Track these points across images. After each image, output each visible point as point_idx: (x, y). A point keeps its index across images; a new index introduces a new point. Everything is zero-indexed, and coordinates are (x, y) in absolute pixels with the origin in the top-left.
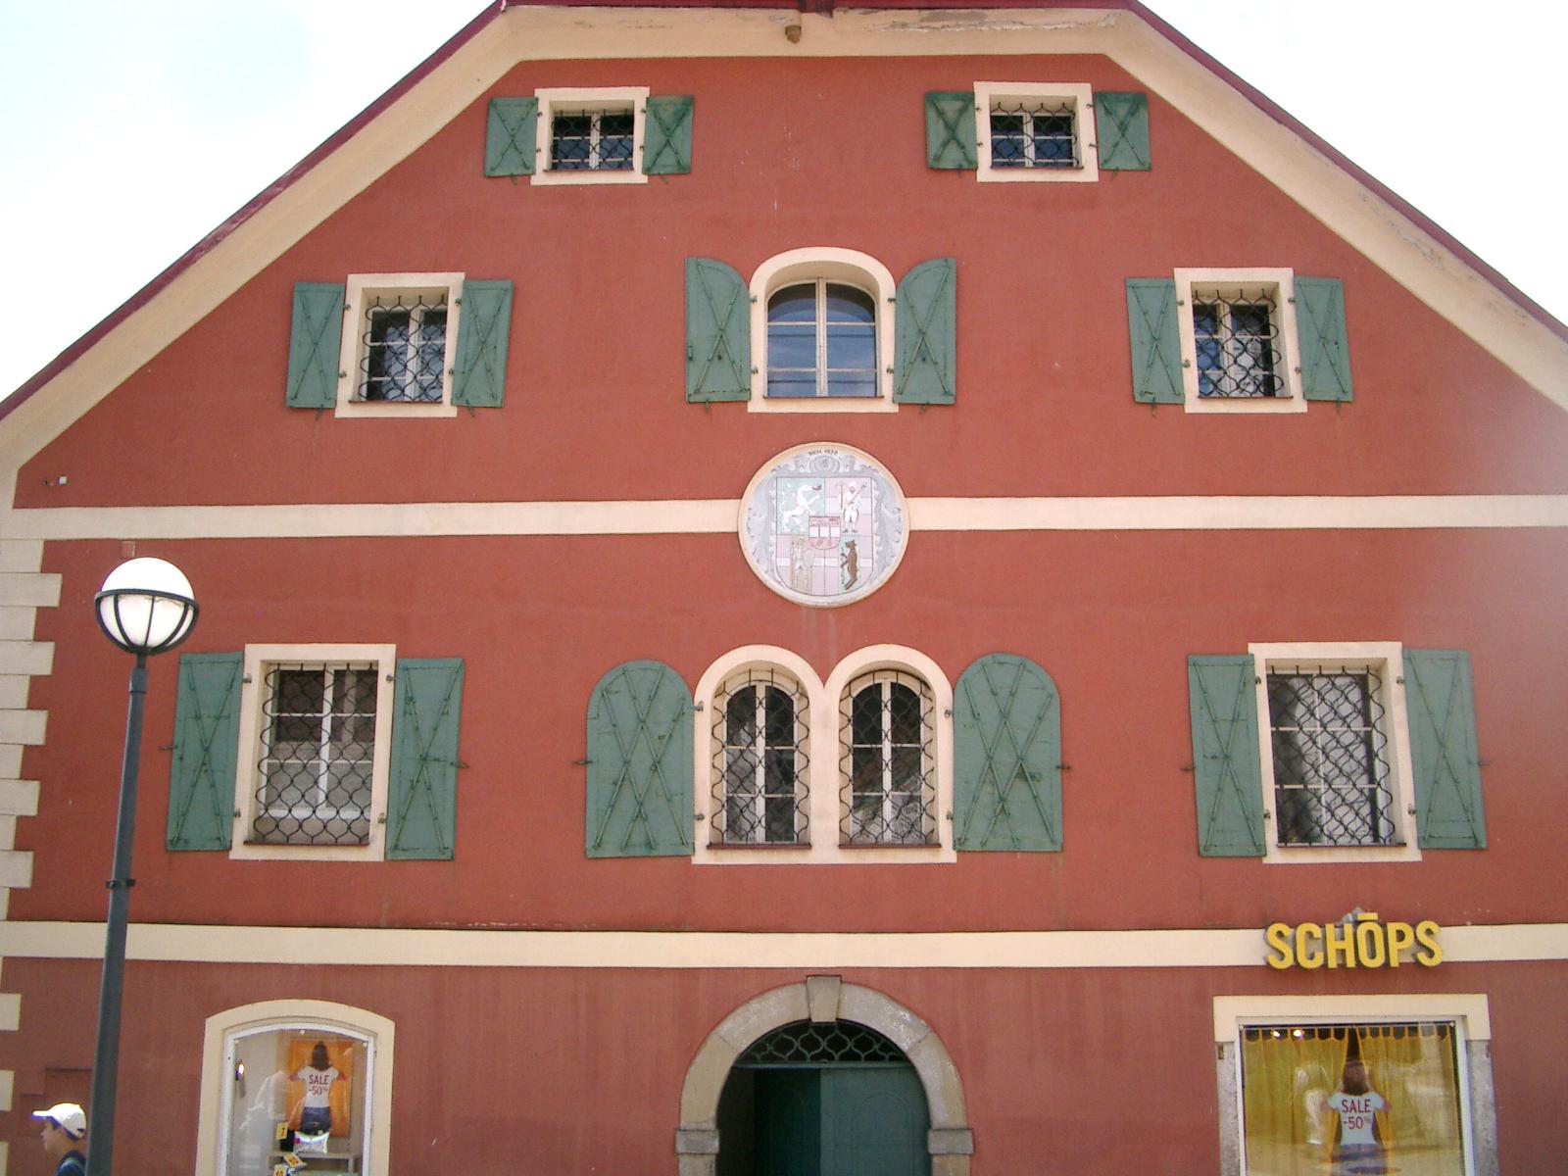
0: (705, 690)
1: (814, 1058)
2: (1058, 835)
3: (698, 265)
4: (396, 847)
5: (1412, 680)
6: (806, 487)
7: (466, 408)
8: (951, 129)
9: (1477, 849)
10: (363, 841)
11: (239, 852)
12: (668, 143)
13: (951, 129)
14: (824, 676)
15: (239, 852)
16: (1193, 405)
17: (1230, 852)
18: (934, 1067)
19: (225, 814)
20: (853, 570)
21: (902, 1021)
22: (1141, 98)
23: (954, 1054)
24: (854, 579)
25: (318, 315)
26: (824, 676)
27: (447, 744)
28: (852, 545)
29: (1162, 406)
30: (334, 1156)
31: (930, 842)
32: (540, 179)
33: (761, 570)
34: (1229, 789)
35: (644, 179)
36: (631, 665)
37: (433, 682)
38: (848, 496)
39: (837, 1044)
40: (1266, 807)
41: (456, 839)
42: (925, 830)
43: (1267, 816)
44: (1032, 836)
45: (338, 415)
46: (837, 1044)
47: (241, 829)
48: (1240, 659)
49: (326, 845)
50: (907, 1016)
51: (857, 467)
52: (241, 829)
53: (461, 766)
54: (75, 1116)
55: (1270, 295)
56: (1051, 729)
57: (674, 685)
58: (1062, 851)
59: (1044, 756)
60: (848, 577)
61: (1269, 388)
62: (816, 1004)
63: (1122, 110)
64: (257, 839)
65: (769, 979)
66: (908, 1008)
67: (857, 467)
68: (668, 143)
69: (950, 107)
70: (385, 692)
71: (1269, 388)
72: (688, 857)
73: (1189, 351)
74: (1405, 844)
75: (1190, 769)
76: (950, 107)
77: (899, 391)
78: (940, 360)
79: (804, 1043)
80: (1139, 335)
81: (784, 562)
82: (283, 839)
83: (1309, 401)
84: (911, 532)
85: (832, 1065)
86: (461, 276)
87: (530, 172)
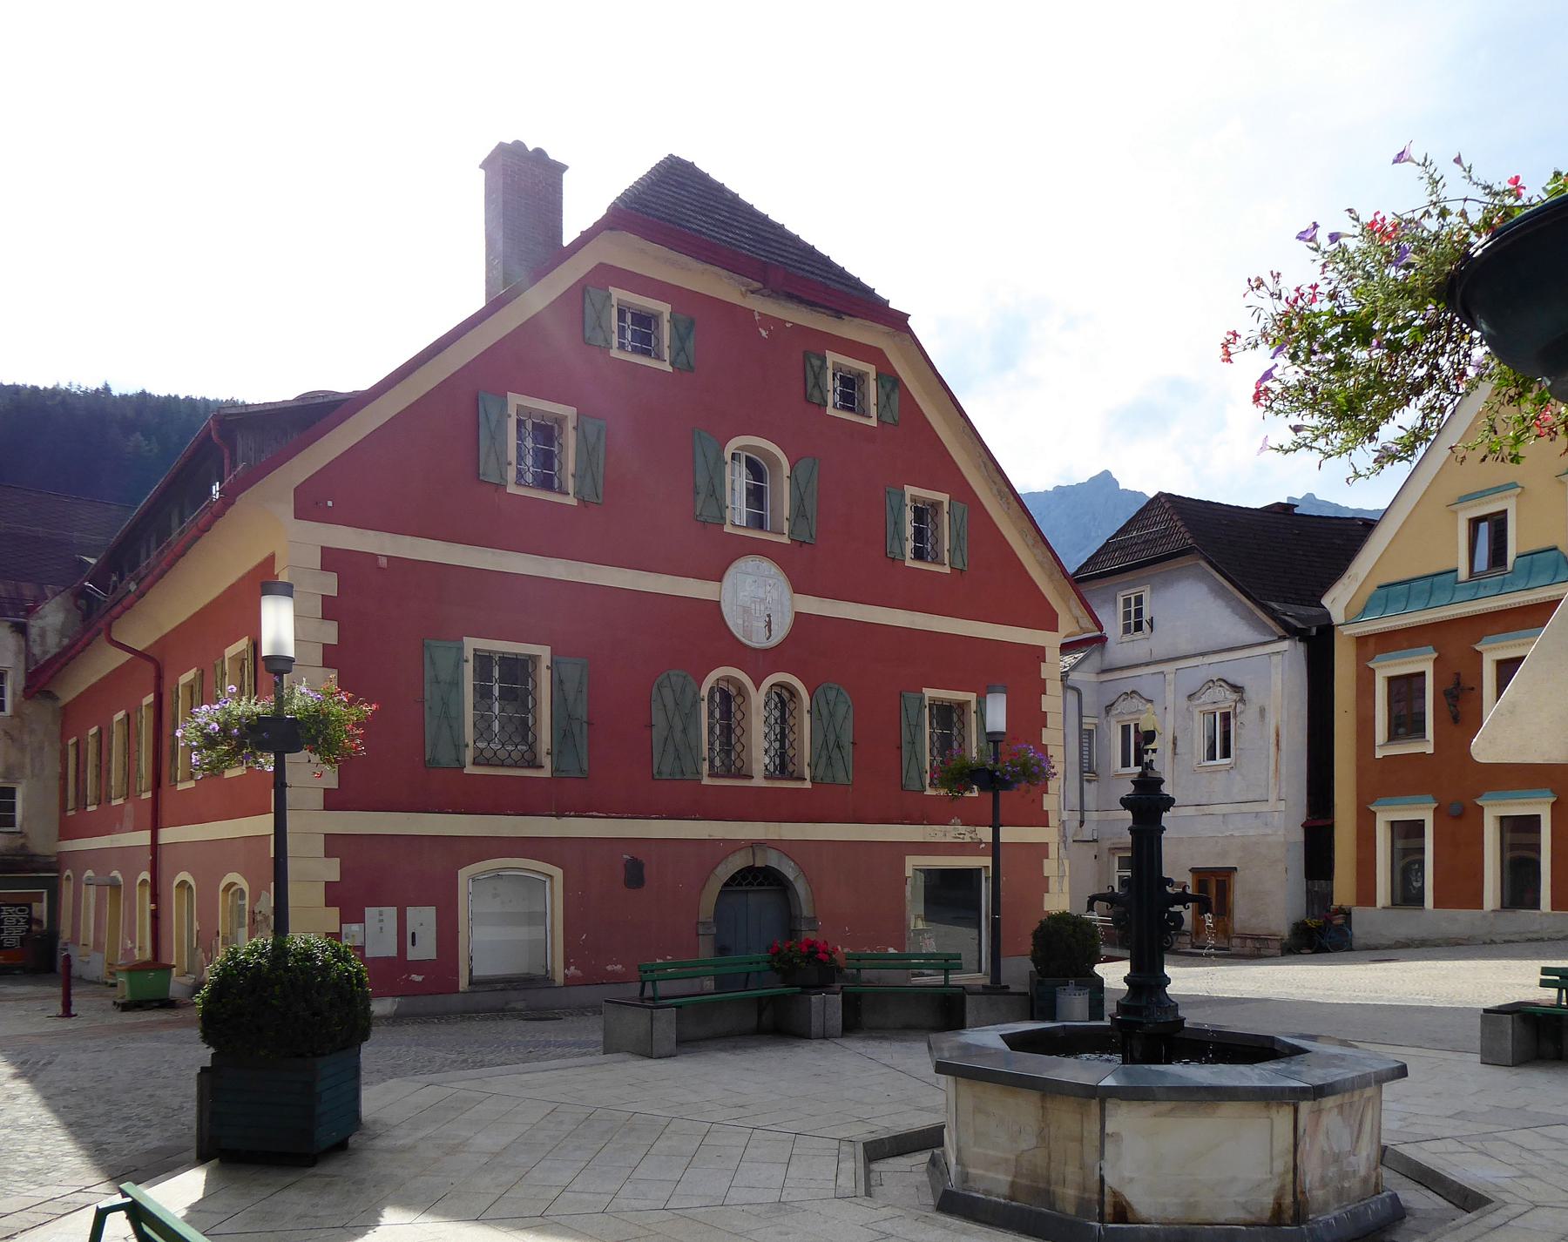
0: (704, 692)
1: (746, 885)
2: (851, 777)
4: (557, 770)
6: (749, 580)
7: (582, 501)
8: (816, 378)
11: (470, 769)
13: (816, 378)
14: (758, 686)
15: (470, 769)
16: (909, 563)
18: (801, 888)
19: (459, 746)
20: (770, 631)
22: (896, 381)
23: (809, 882)
24: (770, 635)
26: (758, 686)
27: (582, 711)
28: (769, 616)
29: (896, 561)
31: (534, 764)
33: (730, 624)
34: (914, 759)
35: (670, 369)
36: (671, 673)
38: (768, 588)
39: (744, 878)
40: (466, 740)
42: (791, 770)
43: (467, 746)
44: (841, 777)
46: (755, 877)
47: (469, 755)
48: (919, 695)
49: (509, 766)
51: (772, 573)
52: (469, 755)
53: (590, 724)
55: (560, 420)
56: (849, 725)
59: (847, 738)
60: (768, 634)
61: (546, 482)
62: (757, 859)
63: (888, 387)
65: (733, 846)
67: (772, 573)
69: (816, 363)
71: (546, 483)
72: (700, 780)
73: (909, 531)
74: (543, 767)
75: (900, 748)
77: (791, 532)
78: (809, 516)
80: (890, 519)
82: (500, 763)
83: (951, 568)
84: (1044, 648)
85: (753, 888)
87: (609, 346)
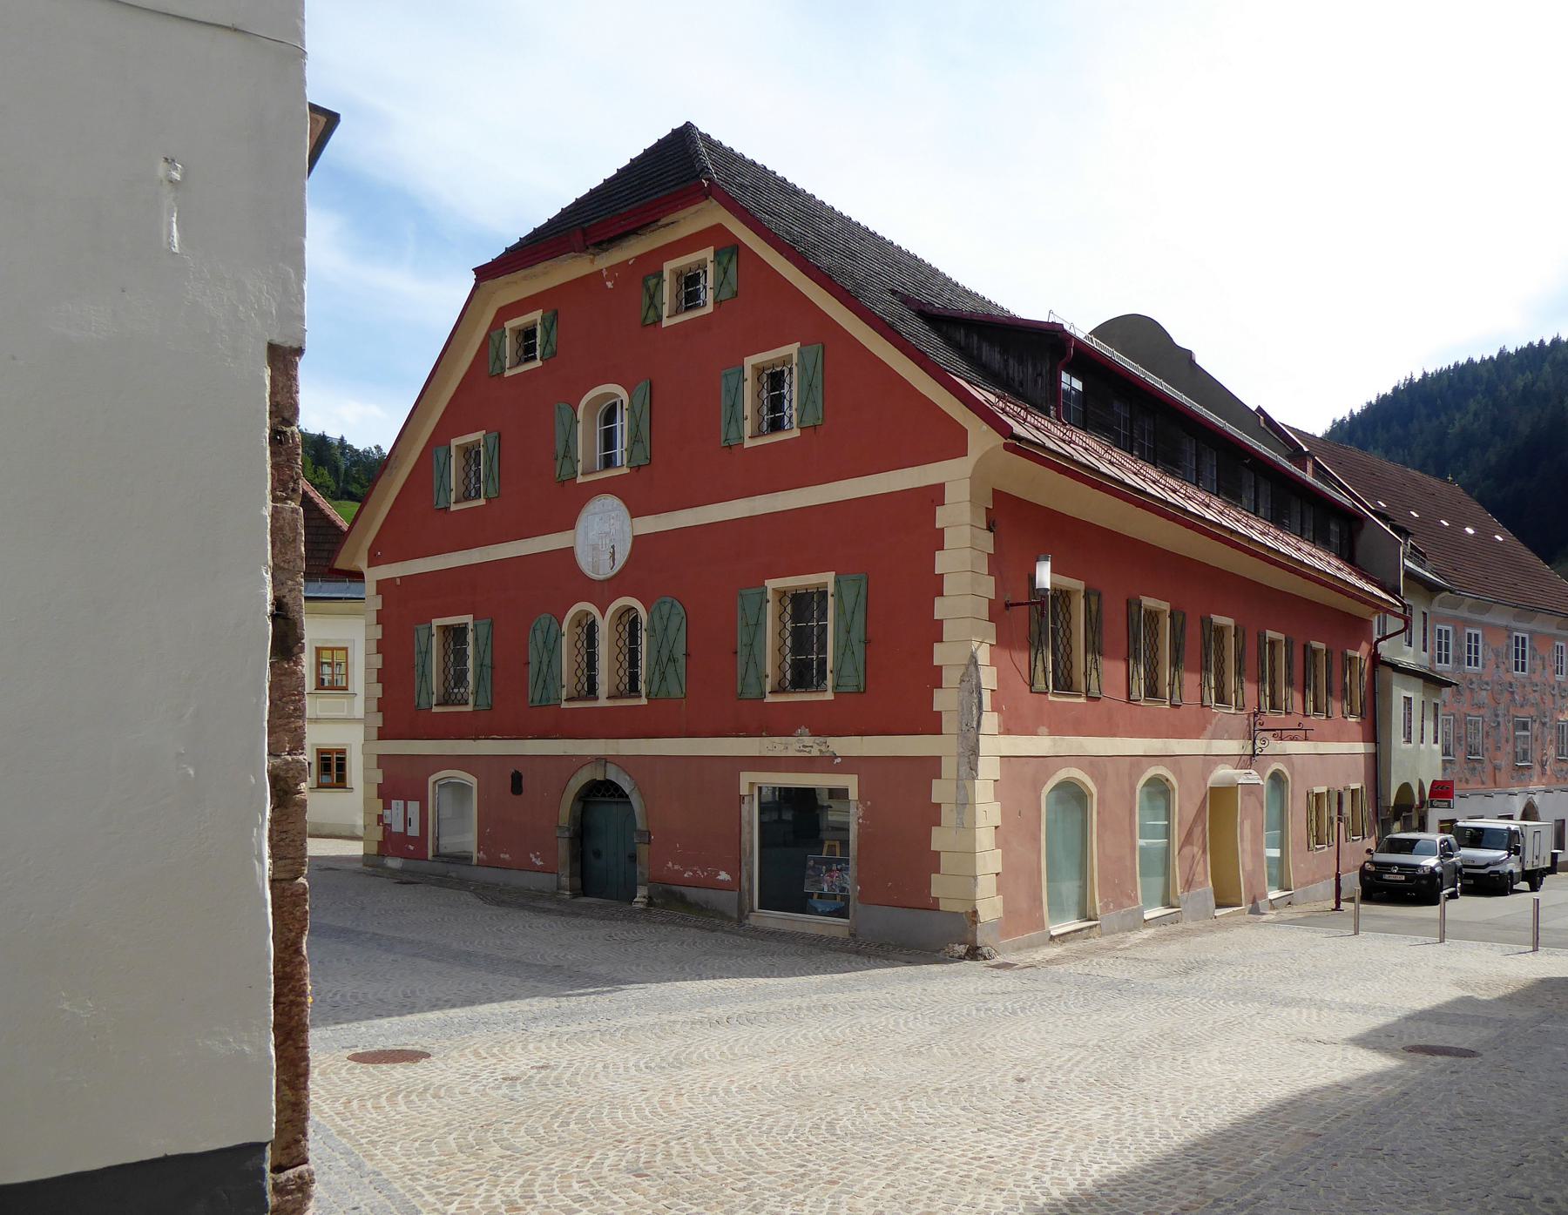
3: (559, 408)
5: (839, 595)
7: (488, 500)
9: (859, 692)
10: (466, 703)
12: (652, 303)
17: (751, 697)
18: (635, 801)
21: (626, 780)
25: (441, 460)
28: (613, 547)
30: (1137, 848)
32: (666, 323)
37: (484, 629)
41: (492, 701)
44: (676, 692)
45: (452, 510)
50: (628, 778)
54: (832, 815)
57: (555, 626)
58: (864, 692)
64: (444, 702)
66: (630, 776)
67: (615, 506)
68: (652, 303)
70: (470, 637)
76: (652, 282)
79: (614, 790)
81: (590, 559)
86: (798, 344)
